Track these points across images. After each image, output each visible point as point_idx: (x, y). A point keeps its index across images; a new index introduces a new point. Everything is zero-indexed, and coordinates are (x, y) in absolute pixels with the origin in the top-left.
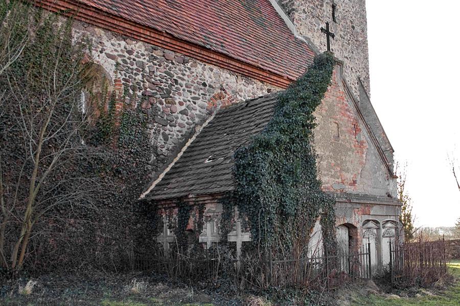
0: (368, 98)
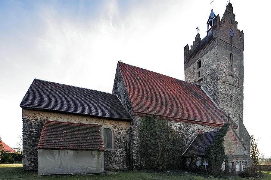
0: (242, 122)
